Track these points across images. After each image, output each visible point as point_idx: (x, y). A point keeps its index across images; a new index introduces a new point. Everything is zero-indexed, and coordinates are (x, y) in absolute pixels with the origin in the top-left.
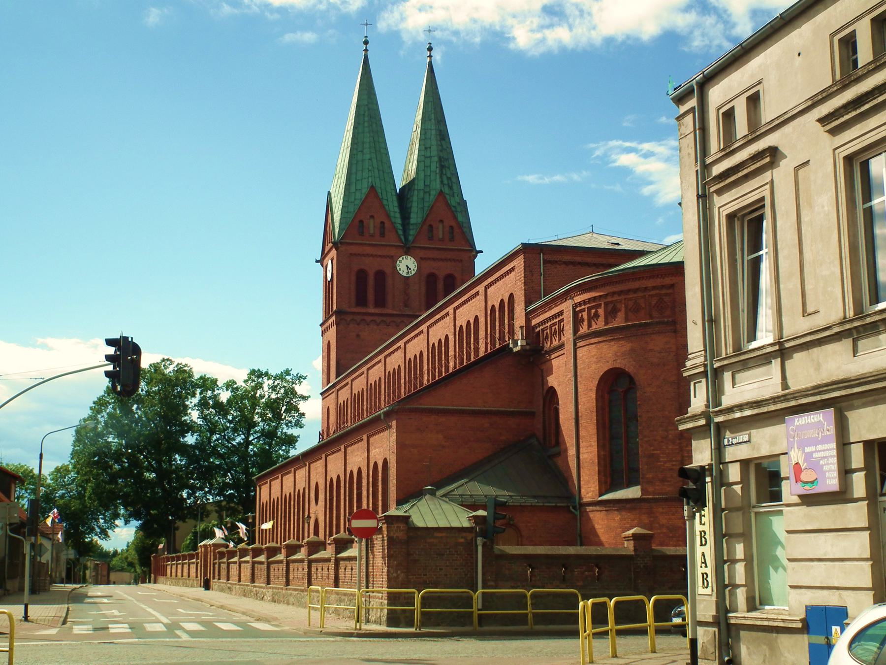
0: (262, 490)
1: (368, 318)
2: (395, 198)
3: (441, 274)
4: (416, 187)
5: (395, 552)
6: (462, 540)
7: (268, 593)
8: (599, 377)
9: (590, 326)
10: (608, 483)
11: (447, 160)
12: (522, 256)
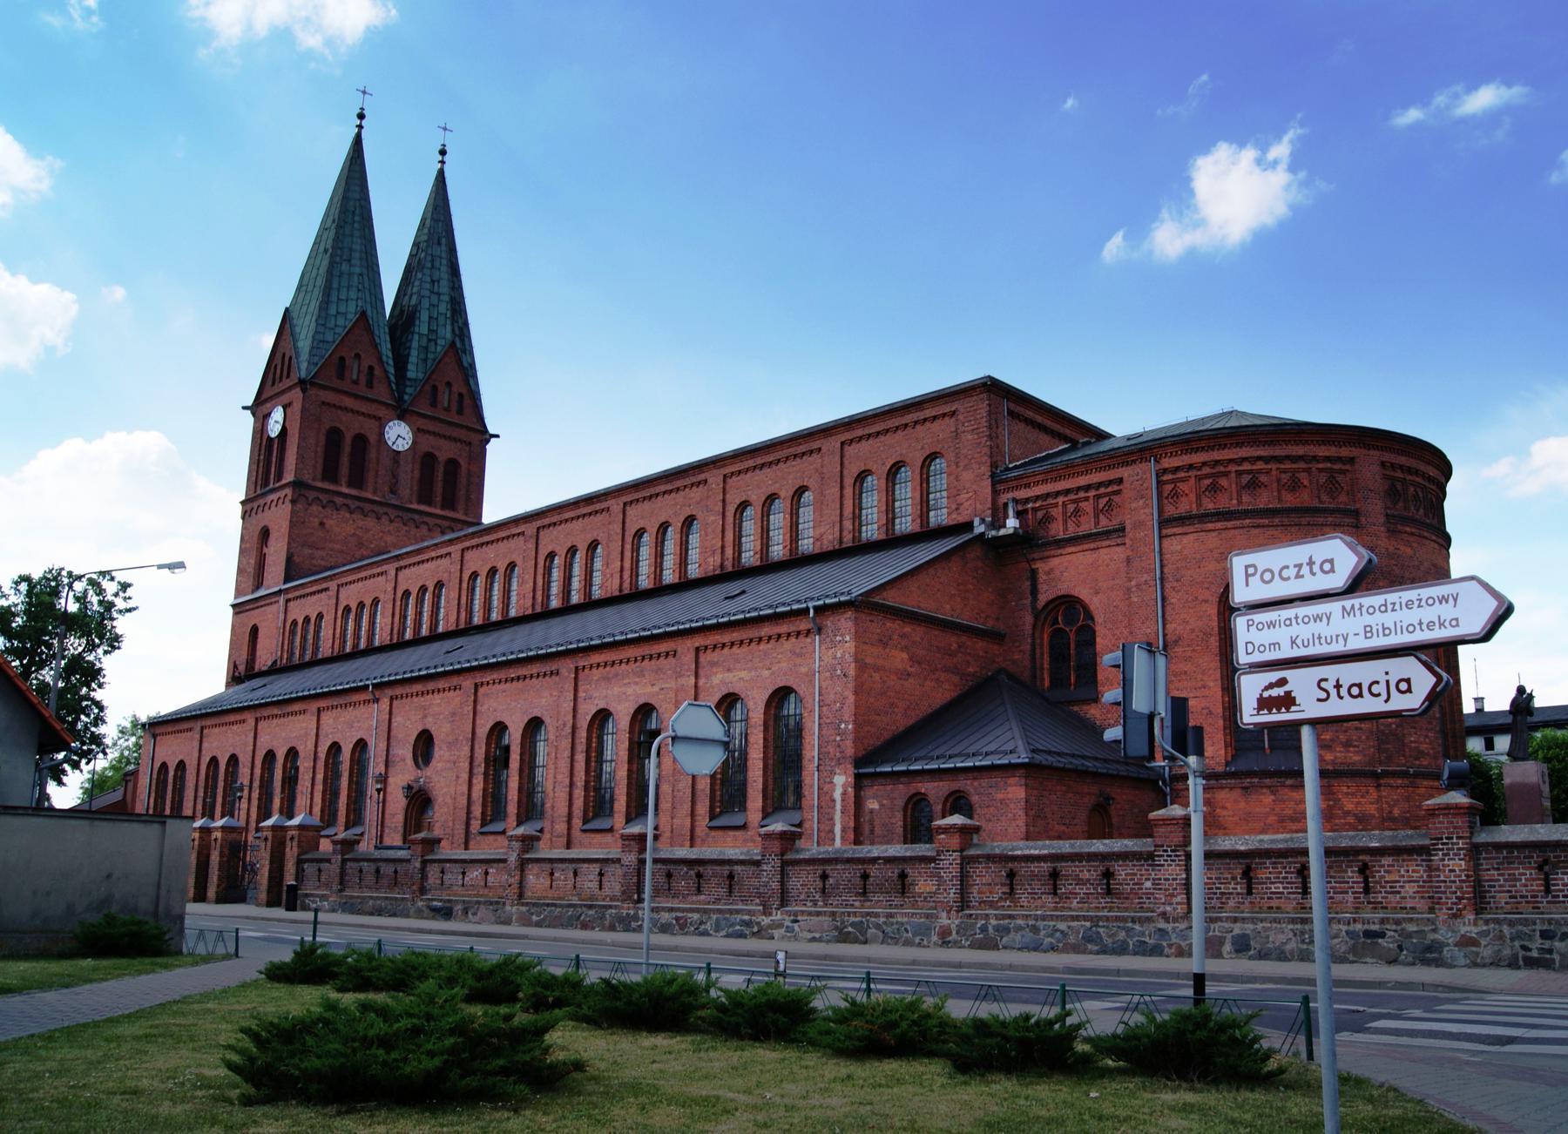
1: (339, 500)
3: (442, 457)
4: (417, 330)
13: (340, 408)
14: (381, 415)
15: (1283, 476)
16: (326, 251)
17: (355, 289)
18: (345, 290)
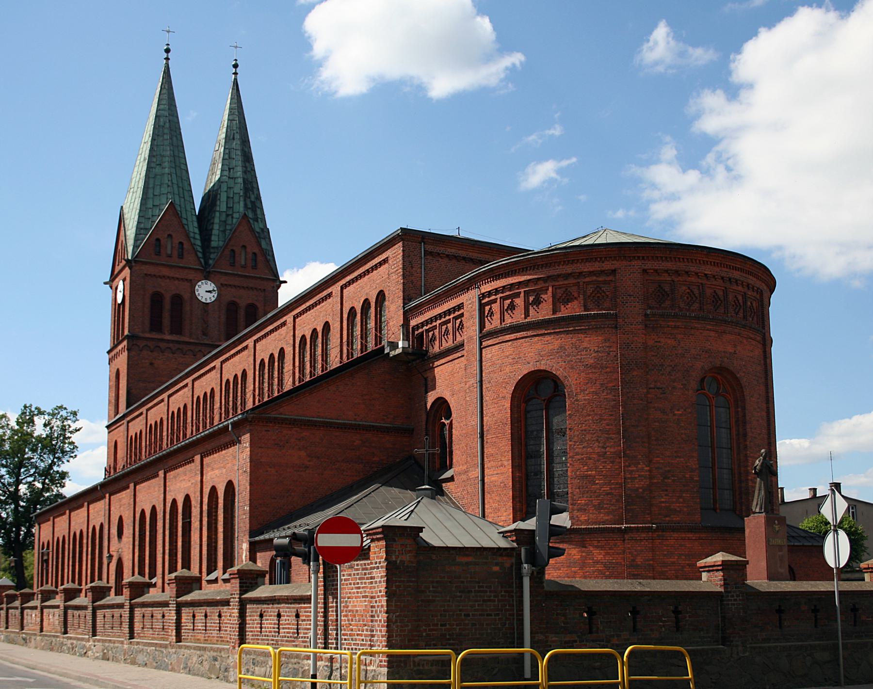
0: (41, 530)
1: (163, 345)
2: (195, 219)
3: (243, 303)
4: (218, 209)
5: (399, 587)
6: (496, 569)
7: (95, 646)
8: (515, 383)
9: (502, 319)
10: (524, 511)
11: (251, 182)
12: (401, 244)
13: (160, 277)
14: (191, 278)
15: (558, 291)
16: (145, 160)
17: (166, 186)
18: (159, 187)
